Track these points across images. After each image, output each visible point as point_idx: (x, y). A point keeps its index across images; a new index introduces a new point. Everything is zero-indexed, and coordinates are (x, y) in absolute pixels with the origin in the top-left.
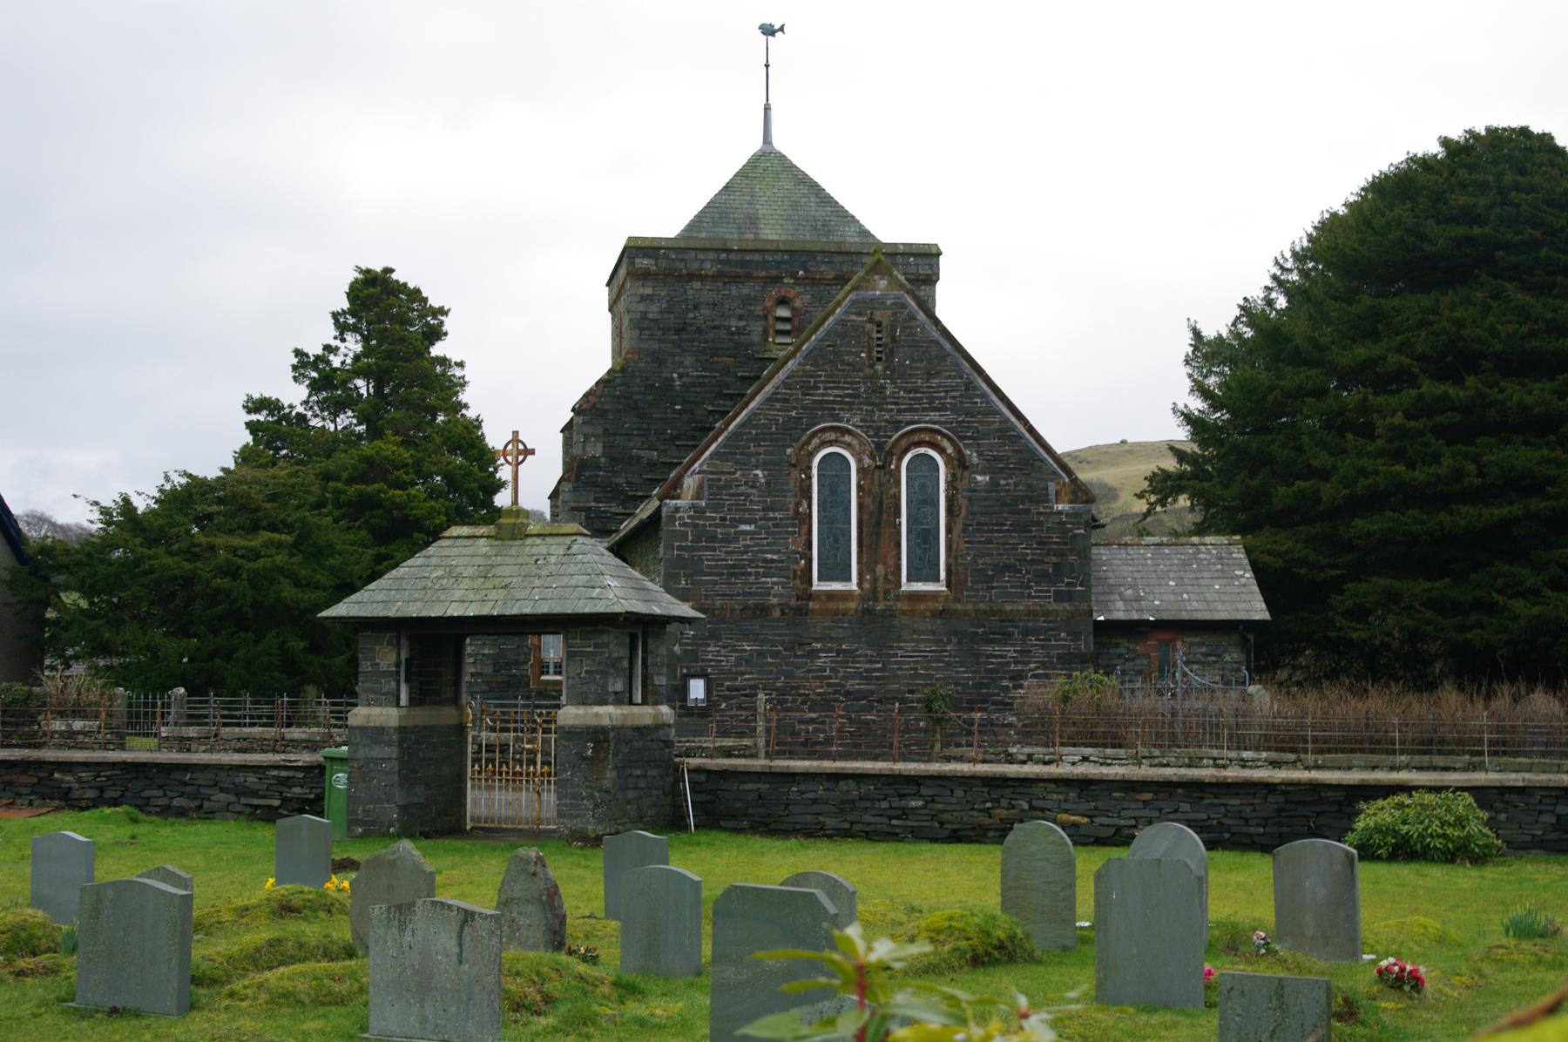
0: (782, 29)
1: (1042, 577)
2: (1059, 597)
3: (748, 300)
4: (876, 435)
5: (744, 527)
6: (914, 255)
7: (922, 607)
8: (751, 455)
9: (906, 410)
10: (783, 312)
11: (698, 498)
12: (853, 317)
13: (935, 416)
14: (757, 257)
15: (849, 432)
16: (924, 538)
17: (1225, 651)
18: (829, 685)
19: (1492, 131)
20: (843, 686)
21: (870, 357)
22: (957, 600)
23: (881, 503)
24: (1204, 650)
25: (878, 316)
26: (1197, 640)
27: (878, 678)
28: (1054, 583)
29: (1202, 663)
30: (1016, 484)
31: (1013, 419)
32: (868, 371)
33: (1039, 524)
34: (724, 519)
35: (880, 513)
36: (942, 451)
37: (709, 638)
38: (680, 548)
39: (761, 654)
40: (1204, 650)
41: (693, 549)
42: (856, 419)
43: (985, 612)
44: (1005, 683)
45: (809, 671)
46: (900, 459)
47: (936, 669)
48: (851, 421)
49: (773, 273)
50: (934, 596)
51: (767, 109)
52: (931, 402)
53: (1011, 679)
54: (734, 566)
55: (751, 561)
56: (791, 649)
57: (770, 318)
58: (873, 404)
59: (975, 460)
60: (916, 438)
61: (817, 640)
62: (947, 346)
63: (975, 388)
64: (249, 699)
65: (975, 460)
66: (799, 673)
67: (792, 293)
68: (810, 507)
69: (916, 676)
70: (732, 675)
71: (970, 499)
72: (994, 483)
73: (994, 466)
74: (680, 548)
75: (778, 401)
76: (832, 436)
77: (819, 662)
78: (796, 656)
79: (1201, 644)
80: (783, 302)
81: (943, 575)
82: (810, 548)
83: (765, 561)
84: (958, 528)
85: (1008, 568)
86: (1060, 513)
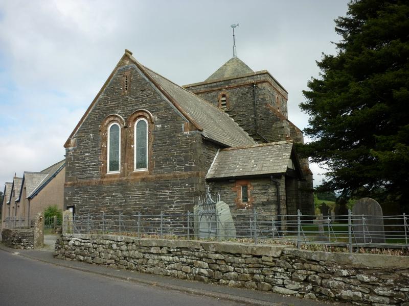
0: (238, 25)
1: (180, 162)
2: (186, 169)
3: (214, 97)
4: (126, 116)
5: (87, 154)
6: (260, 74)
7: (138, 177)
8: (89, 129)
9: (135, 105)
10: (224, 99)
11: (75, 146)
12: (119, 76)
13: (143, 105)
14: (215, 84)
15: (117, 116)
17: (269, 188)
18: (109, 209)
20: (113, 209)
21: (123, 89)
22: (150, 174)
23: (126, 140)
24: (259, 188)
25: (126, 74)
26: (256, 184)
27: (124, 206)
28: (184, 164)
29: (259, 194)
30: (171, 127)
31: (169, 102)
32: (123, 94)
33: (179, 141)
34: (81, 152)
35: (126, 145)
36: (147, 119)
37: (76, 193)
38: (70, 164)
39: (90, 199)
40: (259, 188)
41: (73, 163)
42: (119, 112)
43: (159, 177)
44: (166, 206)
45: (103, 204)
47: (143, 201)
49: (220, 88)
50: (143, 173)
52: (142, 101)
53: (168, 204)
54: (83, 168)
55: (88, 166)
56: (98, 196)
57: (220, 101)
58: (124, 105)
59: (156, 119)
60: (138, 115)
61: (106, 192)
62: (147, 79)
63: (157, 93)
64: (299, 214)
65: (156, 119)
66: (100, 205)
67: (225, 93)
68: (106, 145)
69: (136, 204)
70: (81, 206)
71: (155, 134)
72: (163, 127)
73: (163, 120)
74: (70, 164)
75: (97, 109)
76: (112, 119)
77: (106, 201)
78: (100, 199)
79: (258, 186)
81: (147, 166)
82: (106, 159)
83: (92, 165)
84: (151, 145)
86: (186, 135)
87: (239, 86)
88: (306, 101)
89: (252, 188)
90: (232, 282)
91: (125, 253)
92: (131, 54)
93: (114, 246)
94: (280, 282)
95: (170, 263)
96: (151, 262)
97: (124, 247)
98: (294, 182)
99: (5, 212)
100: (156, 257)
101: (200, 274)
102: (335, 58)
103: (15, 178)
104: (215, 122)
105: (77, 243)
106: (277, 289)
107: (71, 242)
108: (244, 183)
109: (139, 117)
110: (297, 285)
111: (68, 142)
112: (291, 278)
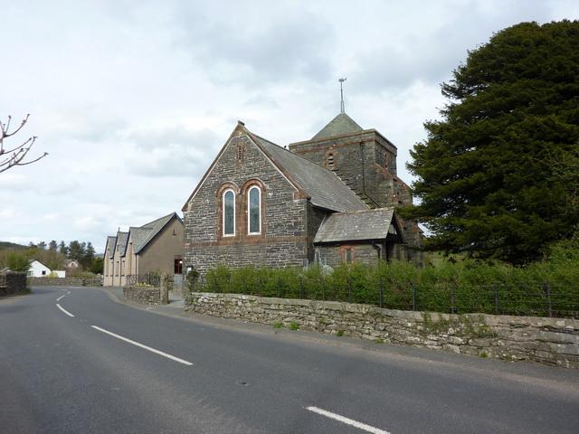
3: (321, 156)
10: (331, 157)
13: (256, 174)
16: (255, 216)
19: (507, 29)
46: (247, 191)
48: (232, 180)
50: (231, 238)
51: (342, 102)
76: (227, 186)
80: (331, 155)
85: (279, 225)
87: (346, 145)
88: (411, 161)
89: (355, 249)
90: (333, 331)
91: (249, 309)
92: (243, 124)
93: (240, 303)
94: (367, 331)
95: (286, 317)
96: (271, 316)
97: (249, 304)
98: (395, 246)
99: (107, 267)
100: (275, 312)
101: (309, 325)
102: (432, 142)
103: (119, 232)
104: (328, 191)
105: (205, 300)
106: (364, 336)
107: (200, 300)
108: (348, 247)
109: (252, 185)
110: (378, 333)
111: (186, 206)
112: (375, 328)
